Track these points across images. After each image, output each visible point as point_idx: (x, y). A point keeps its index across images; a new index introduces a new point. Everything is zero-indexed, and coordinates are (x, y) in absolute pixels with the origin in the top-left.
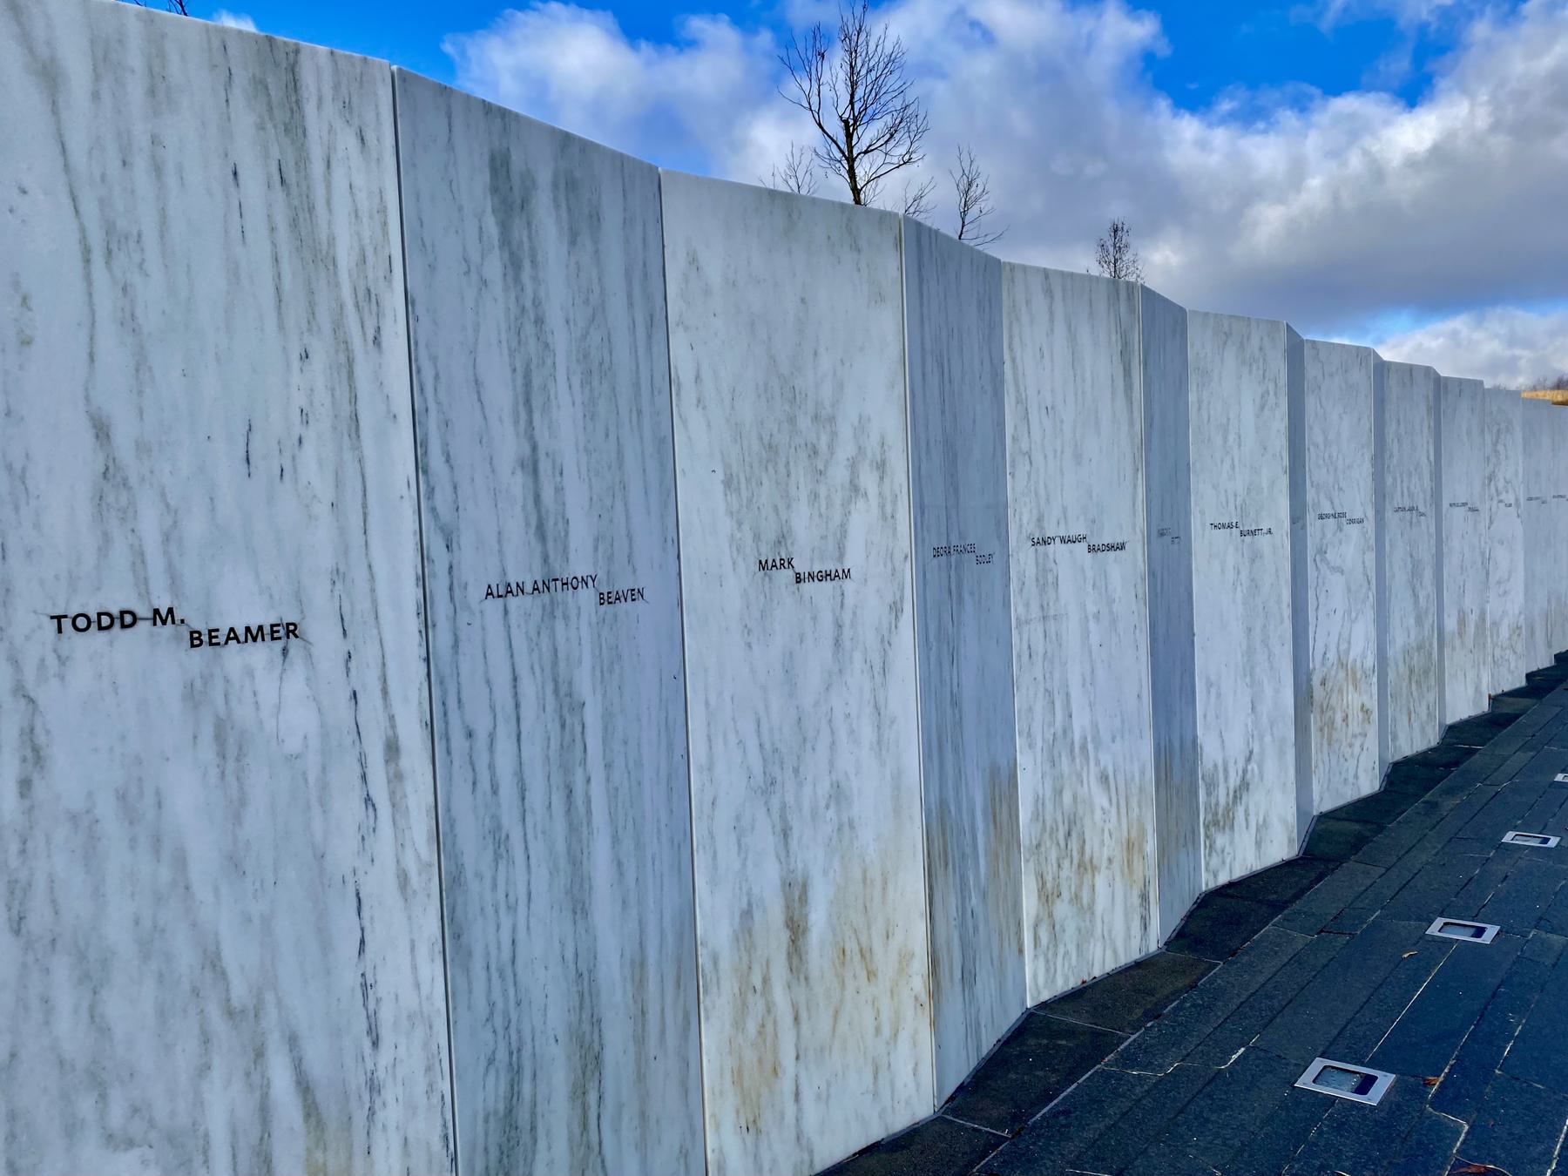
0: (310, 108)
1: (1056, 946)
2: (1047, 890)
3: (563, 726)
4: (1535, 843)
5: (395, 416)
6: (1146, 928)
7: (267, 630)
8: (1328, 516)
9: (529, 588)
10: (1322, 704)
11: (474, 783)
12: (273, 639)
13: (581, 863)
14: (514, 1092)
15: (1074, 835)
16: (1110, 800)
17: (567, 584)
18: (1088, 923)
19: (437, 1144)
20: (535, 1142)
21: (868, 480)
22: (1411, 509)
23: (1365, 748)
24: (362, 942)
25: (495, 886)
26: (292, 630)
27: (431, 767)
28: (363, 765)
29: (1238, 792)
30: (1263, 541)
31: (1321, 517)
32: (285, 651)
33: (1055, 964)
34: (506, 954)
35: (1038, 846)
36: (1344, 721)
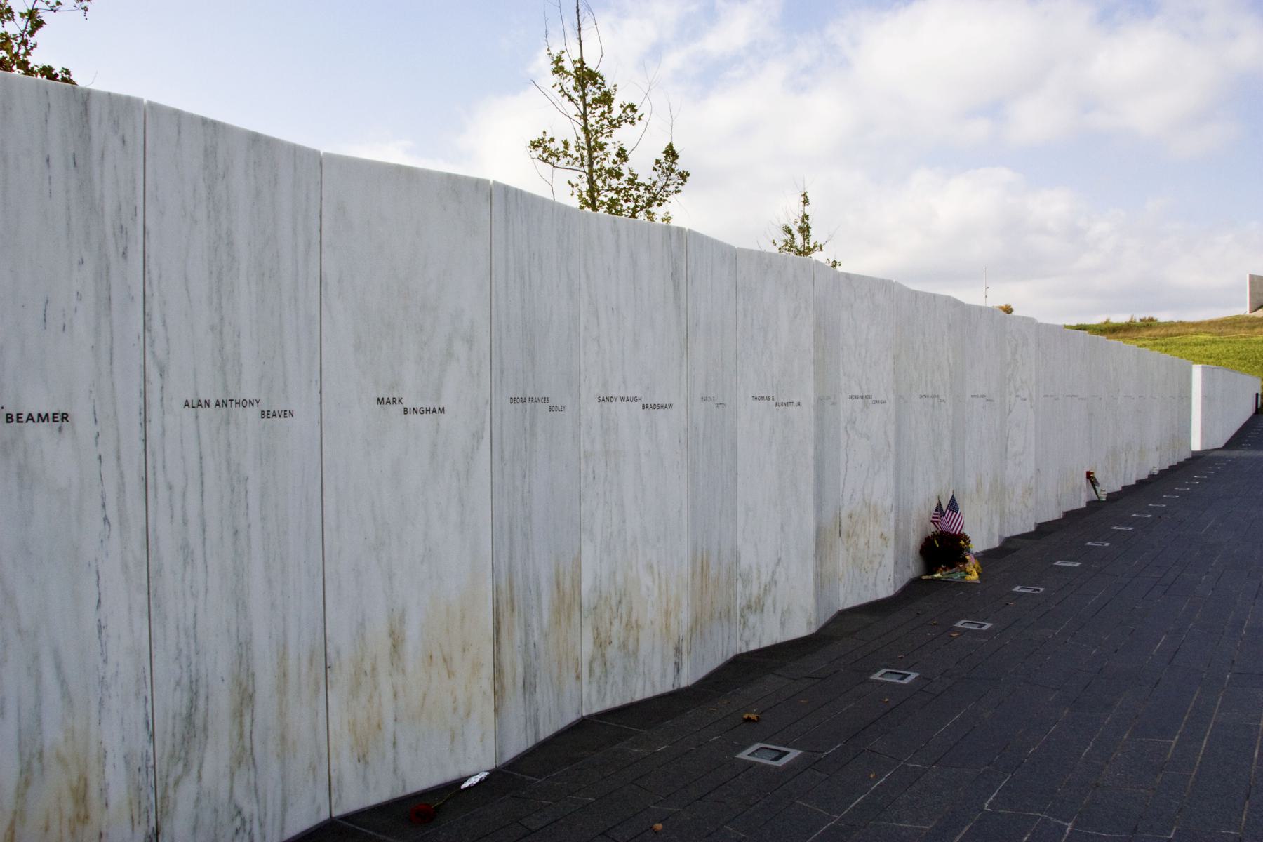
0: (94, 125)
1: (606, 676)
2: (601, 638)
3: (233, 490)
4: (975, 627)
5: (133, 298)
6: (678, 671)
7: (51, 416)
8: (856, 397)
9: (213, 403)
10: (848, 531)
11: (172, 517)
12: (54, 421)
13: (243, 576)
14: (193, 705)
15: (624, 602)
16: (654, 582)
17: (239, 403)
18: (632, 664)
19: (142, 726)
20: (207, 737)
21: (460, 348)
22: (933, 397)
23: (883, 565)
24: (99, 601)
25: (183, 580)
26: (65, 417)
27: (144, 504)
28: (103, 498)
29: (768, 586)
30: (793, 410)
31: (851, 397)
32: (60, 429)
33: (605, 689)
34: (190, 622)
35: (595, 608)
36: (866, 544)
